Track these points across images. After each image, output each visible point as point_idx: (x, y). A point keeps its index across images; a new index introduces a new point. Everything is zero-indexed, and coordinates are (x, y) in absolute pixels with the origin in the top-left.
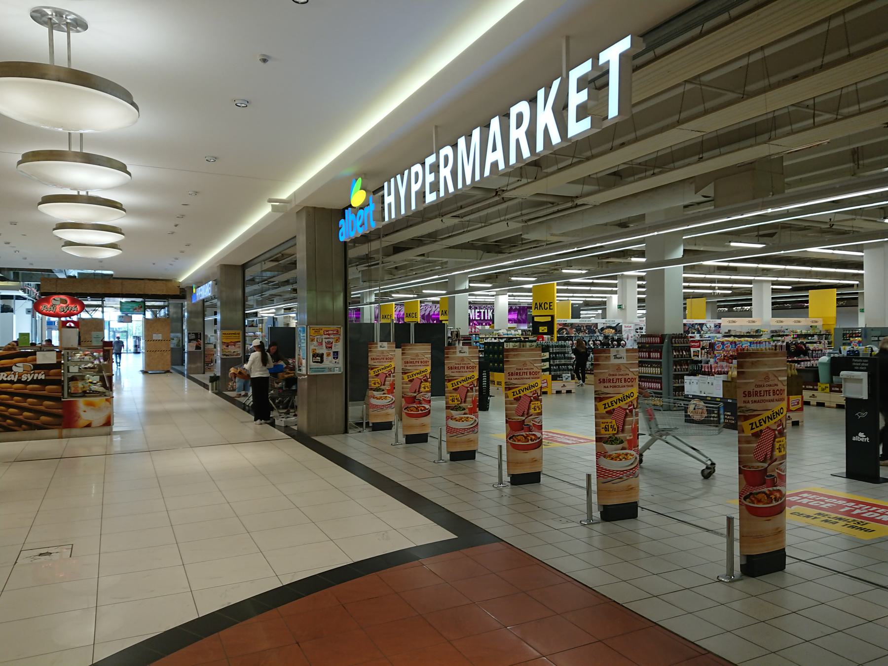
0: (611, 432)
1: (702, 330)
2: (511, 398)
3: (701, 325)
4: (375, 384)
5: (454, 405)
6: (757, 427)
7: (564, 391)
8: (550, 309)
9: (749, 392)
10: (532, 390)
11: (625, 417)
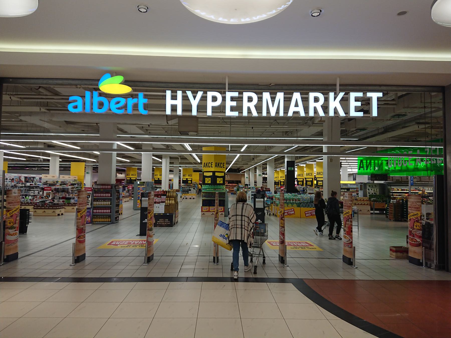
0: (12, 224)
1: (34, 181)
2: (79, 216)
3: (34, 178)
4: (10, 223)
5: (10, 226)
6: (11, 214)
7: (192, 198)
8: (211, 167)
9: (10, 202)
10: (415, 216)
11: (414, 223)
